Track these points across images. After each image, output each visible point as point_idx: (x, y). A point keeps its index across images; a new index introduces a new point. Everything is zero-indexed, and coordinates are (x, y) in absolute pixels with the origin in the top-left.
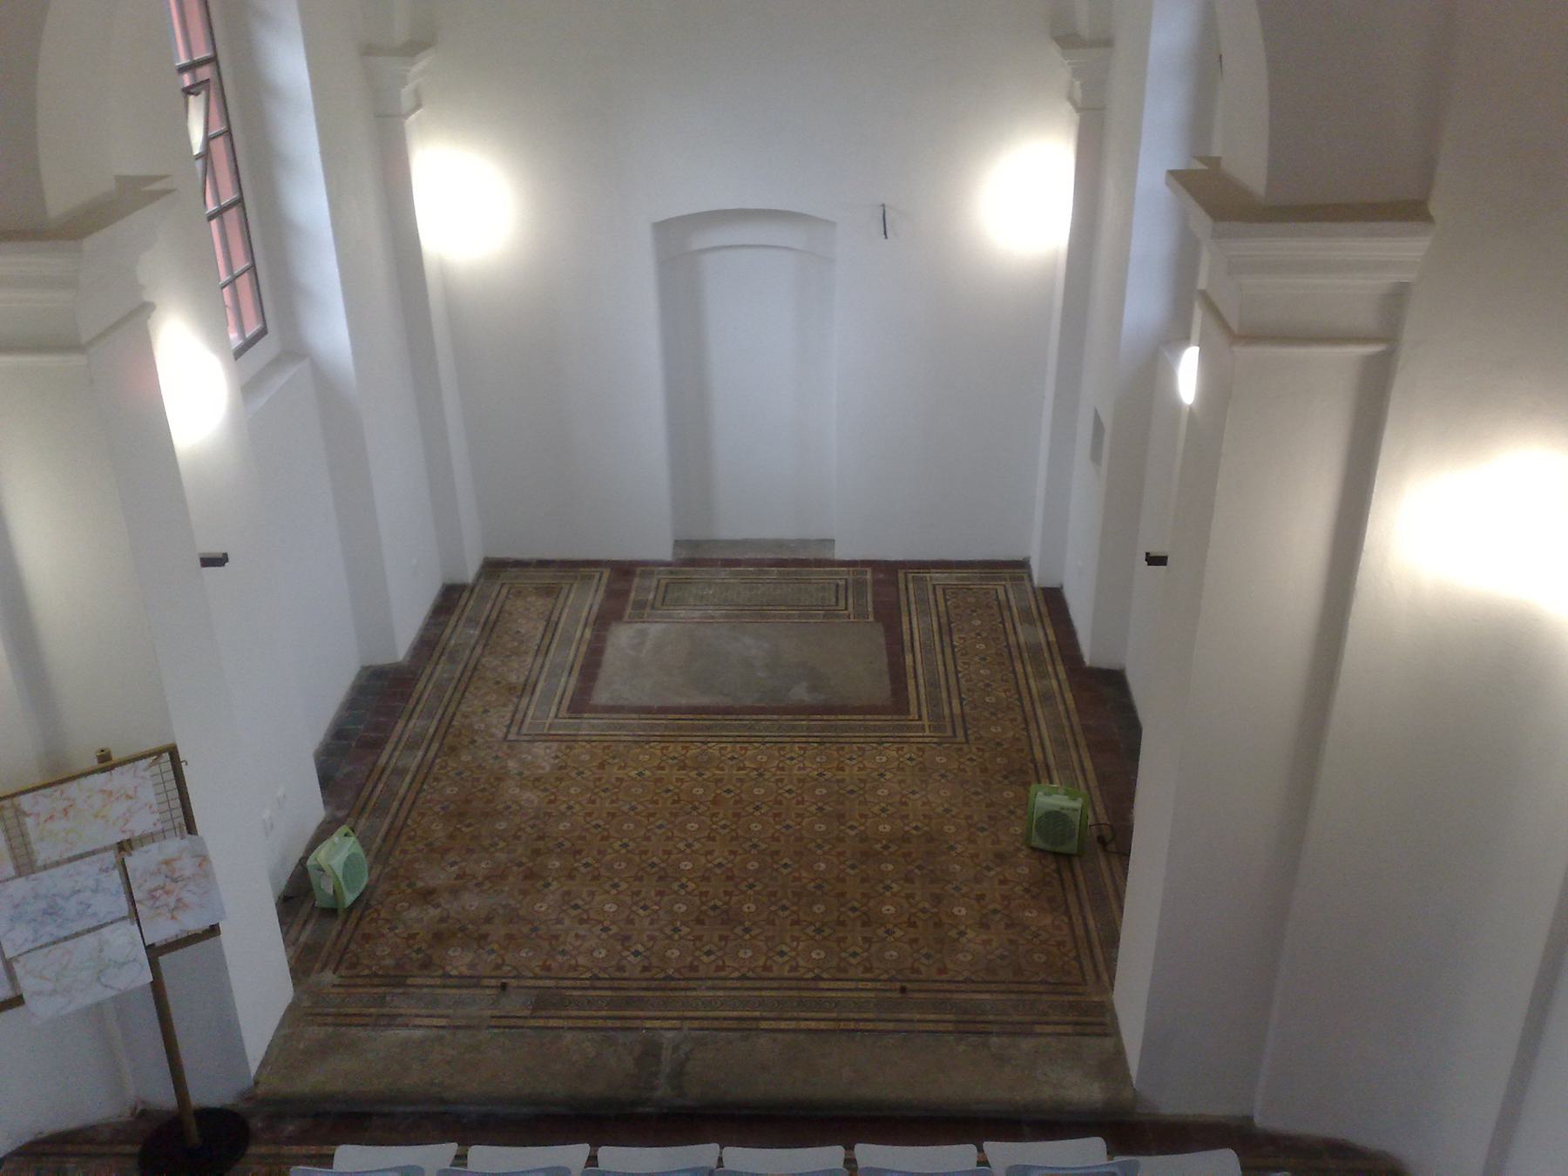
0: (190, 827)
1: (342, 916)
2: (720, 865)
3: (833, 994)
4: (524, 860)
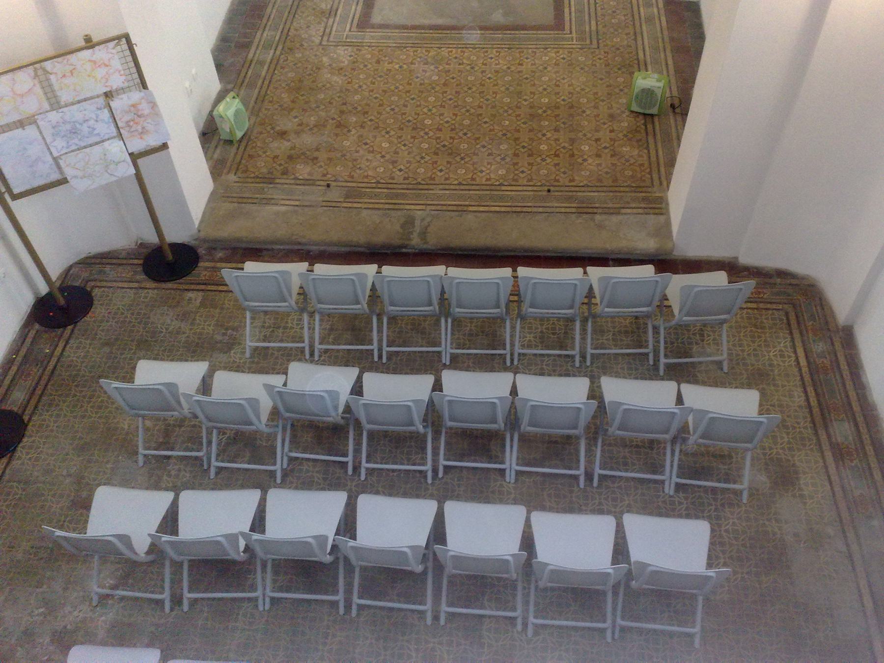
0: (144, 86)
1: (236, 145)
2: (447, 122)
3: (509, 193)
4: (336, 117)
